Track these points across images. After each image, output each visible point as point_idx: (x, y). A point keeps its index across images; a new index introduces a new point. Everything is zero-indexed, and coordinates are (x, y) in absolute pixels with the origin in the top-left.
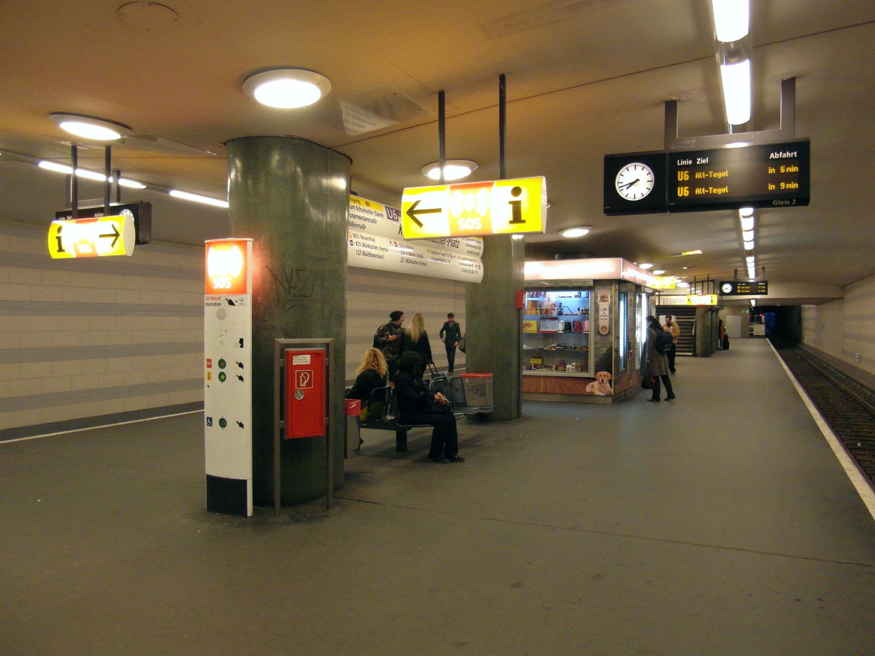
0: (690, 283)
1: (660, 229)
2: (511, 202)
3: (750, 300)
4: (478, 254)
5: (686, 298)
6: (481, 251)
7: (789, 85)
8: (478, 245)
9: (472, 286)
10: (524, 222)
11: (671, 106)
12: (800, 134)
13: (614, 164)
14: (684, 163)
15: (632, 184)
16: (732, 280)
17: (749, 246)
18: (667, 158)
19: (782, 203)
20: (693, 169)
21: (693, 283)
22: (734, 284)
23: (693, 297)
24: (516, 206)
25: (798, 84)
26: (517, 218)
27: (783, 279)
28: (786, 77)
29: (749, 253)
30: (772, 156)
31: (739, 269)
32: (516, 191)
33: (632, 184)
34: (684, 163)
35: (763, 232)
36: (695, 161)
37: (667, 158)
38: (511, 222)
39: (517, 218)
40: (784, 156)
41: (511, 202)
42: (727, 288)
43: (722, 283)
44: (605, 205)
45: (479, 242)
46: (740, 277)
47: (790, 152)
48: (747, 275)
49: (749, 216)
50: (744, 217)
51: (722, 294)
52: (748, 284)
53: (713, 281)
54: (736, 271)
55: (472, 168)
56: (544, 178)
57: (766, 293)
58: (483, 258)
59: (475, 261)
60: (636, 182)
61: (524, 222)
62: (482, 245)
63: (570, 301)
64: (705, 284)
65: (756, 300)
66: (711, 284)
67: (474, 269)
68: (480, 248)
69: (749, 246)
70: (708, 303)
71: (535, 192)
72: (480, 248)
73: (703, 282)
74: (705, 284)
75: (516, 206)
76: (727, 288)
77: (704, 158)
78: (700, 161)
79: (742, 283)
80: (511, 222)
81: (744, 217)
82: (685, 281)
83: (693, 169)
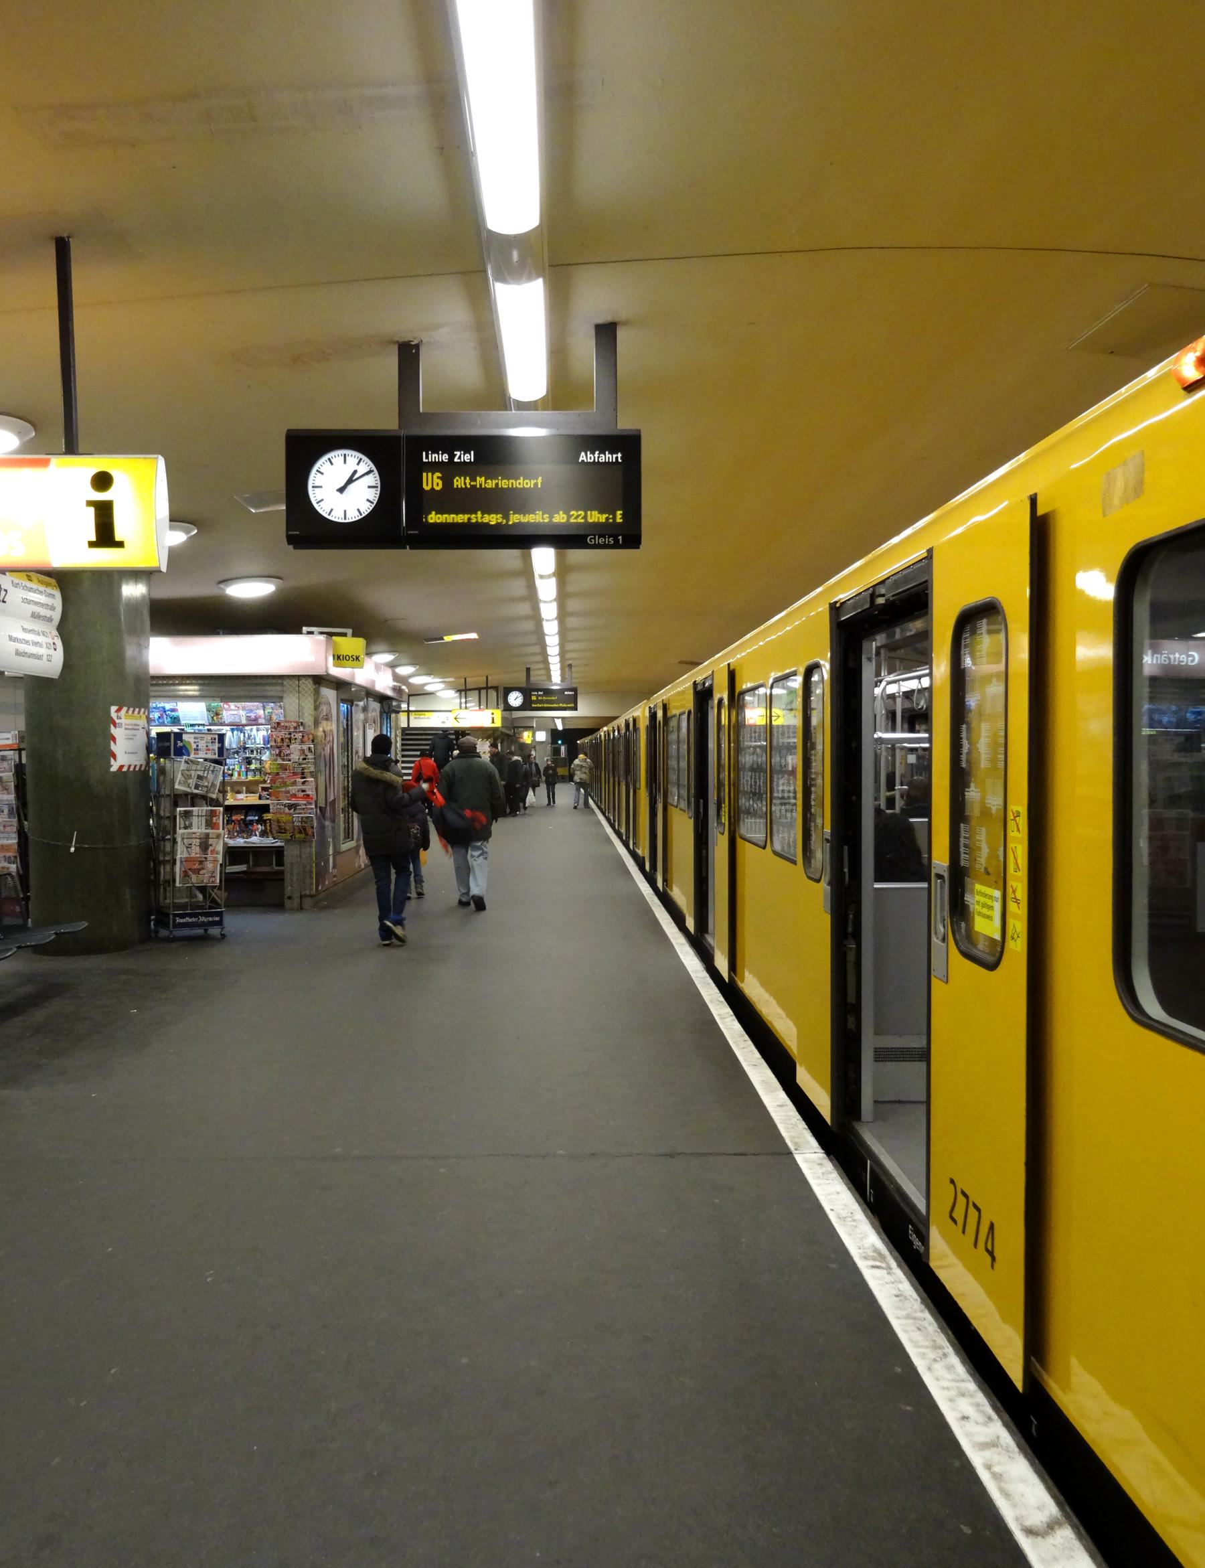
0: (460, 691)
1: (400, 584)
2: (90, 503)
3: (553, 718)
4: (50, 620)
5: (451, 716)
6: (57, 615)
7: (606, 333)
8: (49, 601)
9: (37, 686)
10: (120, 544)
11: (409, 355)
12: (625, 424)
13: (305, 449)
14: (434, 457)
15: (350, 481)
16: (384, 419)
17: (511, 199)
18: (403, 444)
19: (601, 541)
20: (449, 470)
21: (464, 691)
22: (526, 692)
23: (463, 713)
24: (104, 513)
25: (621, 334)
26: (105, 536)
27: (602, 689)
28: (600, 321)
29: (515, 256)
30: (582, 457)
31: (532, 667)
32: (102, 481)
33: (350, 481)
34: (434, 457)
35: (572, 622)
36: (452, 456)
37: (403, 444)
38: (92, 544)
39: (105, 536)
40: (602, 459)
41: (90, 503)
42: (515, 699)
43: (508, 690)
44: (288, 529)
45: (53, 596)
46: (537, 677)
47: (612, 453)
48: (549, 677)
49: (549, 577)
50: (541, 577)
51: (508, 708)
52: (548, 692)
53: (496, 688)
54: (528, 670)
55: (19, 434)
56: (161, 462)
57: (575, 709)
58: (62, 629)
59: (44, 633)
60: (343, 488)
61: (120, 544)
62: (58, 602)
63: (995, 802)
64: (483, 692)
65: (563, 718)
66: (493, 694)
67: (43, 651)
68: (53, 608)
69: (511, 199)
70: (487, 724)
71: (143, 492)
72: (53, 608)
73: (479, 689)
74: (483, 692)
75: (104, 513)
76: (515, 699)
77: (467, 451)
78: (462, 457)
79: (450, 444)
80: (92, 544)
81: (541, 577)
82: (450, 686)
83: (449, 470)
